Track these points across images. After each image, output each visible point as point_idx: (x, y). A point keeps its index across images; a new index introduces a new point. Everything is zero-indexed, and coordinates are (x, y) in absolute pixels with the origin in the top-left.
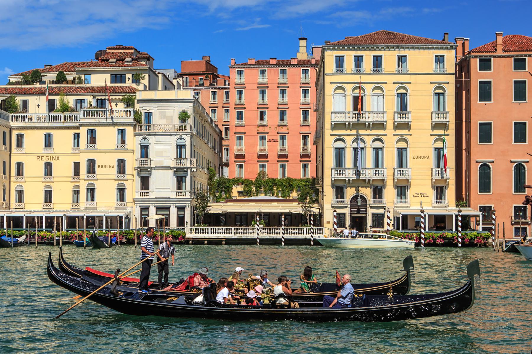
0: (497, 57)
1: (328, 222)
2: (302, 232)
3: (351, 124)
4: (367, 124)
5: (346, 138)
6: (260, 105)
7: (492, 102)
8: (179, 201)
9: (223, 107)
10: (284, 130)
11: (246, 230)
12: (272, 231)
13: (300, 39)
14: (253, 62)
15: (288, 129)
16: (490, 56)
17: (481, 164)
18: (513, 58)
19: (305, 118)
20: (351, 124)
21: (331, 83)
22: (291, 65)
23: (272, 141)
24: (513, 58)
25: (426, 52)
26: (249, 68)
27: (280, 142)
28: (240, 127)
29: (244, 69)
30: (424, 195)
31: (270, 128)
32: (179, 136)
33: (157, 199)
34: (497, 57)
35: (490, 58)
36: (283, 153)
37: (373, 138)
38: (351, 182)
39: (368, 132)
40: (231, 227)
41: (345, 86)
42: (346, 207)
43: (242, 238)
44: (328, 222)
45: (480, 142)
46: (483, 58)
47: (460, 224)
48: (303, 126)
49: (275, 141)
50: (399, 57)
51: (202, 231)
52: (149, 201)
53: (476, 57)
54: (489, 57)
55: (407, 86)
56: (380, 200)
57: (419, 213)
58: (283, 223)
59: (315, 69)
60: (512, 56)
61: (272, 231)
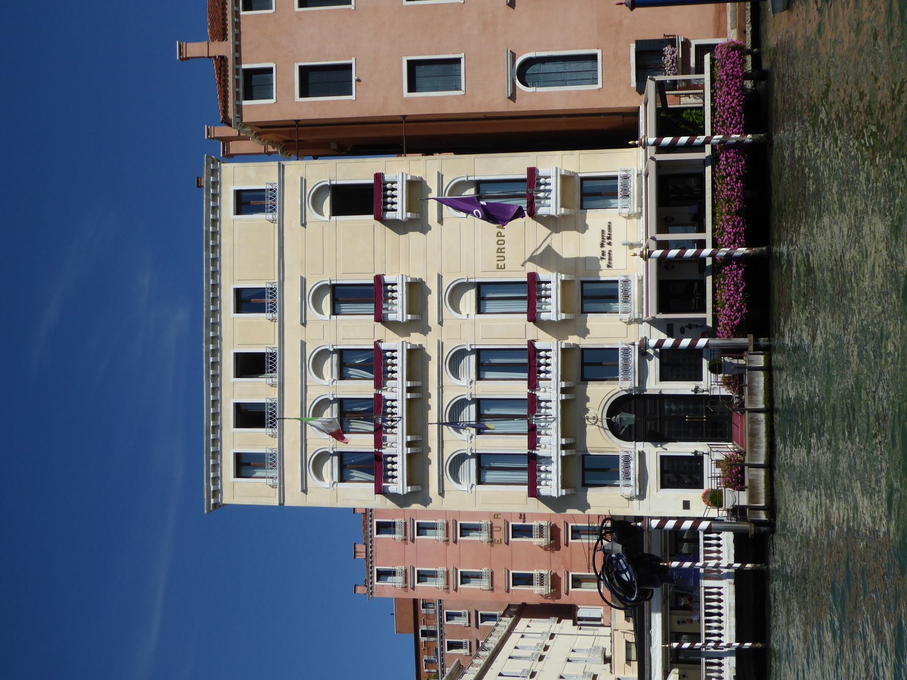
0: (237, 55)
1: (686, 505)
3: (409, 438)
4: (409, 396)
6: (447, 536)
7: (353, 61)
11: (709, 628)
12: (713, 600)
14: (361, 548)
16: (237, 71)
17: (518, 83)
18: (242, 13)
21: (305, 491)
24: (242, 13)
25: (226, 240)
29: (375, 568)
30: (606, 235)
34: (237, 55)
35: (241, 72)
37: (448, 376)
38: (570, 441)
39: (433, 389)
40: (702, 590)
41: (311, 453)
42: (642, 455)
44: (686, 505)
45: (459, 89)
46: (241, 90)
47: (683, 140)
50: (239, 309)
53: (239, 109)
54: (238, 74)
55: (311, 286)
56: (619, 190)
57: (653, 263)
58: (687, 565)
60: (237, 14)
61: (713, 600)
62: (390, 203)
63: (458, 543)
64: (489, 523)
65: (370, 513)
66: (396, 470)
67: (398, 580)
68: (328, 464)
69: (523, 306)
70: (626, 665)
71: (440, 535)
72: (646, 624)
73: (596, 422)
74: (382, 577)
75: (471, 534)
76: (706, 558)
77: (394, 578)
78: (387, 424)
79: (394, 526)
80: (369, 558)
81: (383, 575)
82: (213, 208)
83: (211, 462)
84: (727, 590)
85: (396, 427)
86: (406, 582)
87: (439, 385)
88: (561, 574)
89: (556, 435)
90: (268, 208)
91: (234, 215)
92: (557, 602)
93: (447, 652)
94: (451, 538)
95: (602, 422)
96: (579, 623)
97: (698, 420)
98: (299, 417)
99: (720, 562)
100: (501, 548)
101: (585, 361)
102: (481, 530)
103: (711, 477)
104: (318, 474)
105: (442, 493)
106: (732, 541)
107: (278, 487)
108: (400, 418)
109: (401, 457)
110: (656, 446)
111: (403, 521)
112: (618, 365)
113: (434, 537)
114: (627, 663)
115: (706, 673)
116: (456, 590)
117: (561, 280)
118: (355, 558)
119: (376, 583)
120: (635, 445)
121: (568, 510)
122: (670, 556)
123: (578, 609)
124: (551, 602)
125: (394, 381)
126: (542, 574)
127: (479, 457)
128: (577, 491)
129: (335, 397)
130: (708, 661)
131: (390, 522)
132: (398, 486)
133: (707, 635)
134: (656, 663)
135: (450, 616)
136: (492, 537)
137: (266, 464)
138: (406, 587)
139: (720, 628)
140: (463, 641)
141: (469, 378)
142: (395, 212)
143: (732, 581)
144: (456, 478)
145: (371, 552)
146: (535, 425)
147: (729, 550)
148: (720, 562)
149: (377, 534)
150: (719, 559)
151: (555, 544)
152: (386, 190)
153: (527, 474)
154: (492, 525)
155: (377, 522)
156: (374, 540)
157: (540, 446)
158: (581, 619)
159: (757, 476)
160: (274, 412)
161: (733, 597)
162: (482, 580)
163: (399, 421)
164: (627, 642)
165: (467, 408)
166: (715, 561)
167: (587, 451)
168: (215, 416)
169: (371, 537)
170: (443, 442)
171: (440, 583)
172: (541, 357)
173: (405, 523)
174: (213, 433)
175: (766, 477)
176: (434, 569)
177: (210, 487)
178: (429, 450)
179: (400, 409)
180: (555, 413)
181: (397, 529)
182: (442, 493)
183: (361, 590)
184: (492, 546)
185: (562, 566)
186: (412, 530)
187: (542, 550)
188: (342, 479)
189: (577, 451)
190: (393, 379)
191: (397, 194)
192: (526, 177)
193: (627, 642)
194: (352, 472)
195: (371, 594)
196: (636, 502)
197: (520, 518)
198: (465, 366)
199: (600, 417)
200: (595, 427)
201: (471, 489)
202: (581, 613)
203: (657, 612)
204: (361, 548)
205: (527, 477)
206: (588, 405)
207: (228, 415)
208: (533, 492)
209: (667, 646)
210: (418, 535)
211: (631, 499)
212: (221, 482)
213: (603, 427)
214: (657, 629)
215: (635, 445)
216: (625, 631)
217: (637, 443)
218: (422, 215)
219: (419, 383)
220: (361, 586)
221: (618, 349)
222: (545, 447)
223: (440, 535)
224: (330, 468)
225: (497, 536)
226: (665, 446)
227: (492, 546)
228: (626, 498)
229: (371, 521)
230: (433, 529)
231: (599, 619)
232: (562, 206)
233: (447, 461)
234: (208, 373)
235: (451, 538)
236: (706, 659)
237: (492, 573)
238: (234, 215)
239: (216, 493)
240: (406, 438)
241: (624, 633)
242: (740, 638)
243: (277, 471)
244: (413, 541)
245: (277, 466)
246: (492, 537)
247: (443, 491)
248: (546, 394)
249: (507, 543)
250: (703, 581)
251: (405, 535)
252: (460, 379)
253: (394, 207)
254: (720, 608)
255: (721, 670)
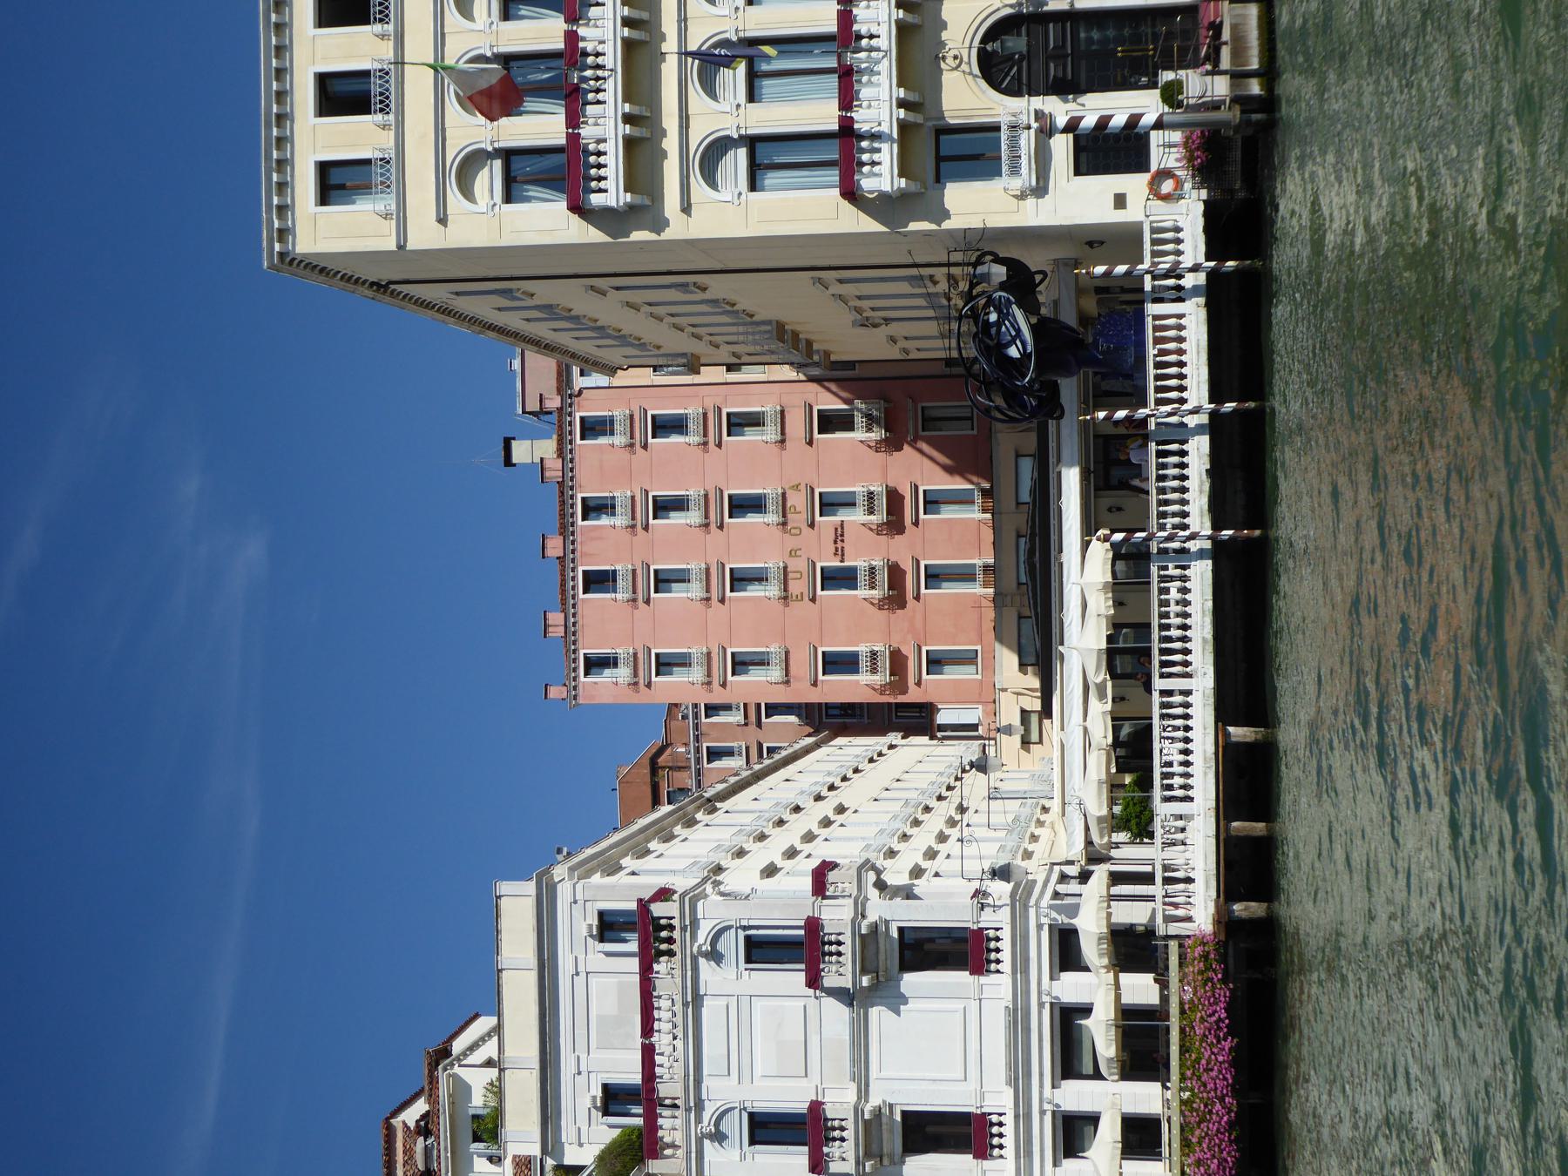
1: (1120, 201)
2: (1172, 321)
3: (627, 107)
5: (700, 133)
6: (708, 591)
8: (1026, 960)
9: (759, 724)
10: (797, 500)
13: (508, 461)
15: (796, 487)
19: (755, 420)
20: (627, 107)
21: (442, 220)
22: (567, 479)
23: (839, 545)
26: (579, 634)
27: (844, 516)
28: (792, 662)
29: (582, 652)
31: (793, 553)
32: (702, 961)
33: (1019, 1075)
36: (882, 503)
38: (913, 97)
39: (670, 122)
43: (1209, 636)
44: (1120, 201)
48: (783, 433)
49: (839, 533)
51: (1172, 358)
52: (1028, 1116)
59: (580, 392)
61: (1174, 664)
62: (592, 154)
63: (727, 602)
64: (781, 565)
65: (572, 556)
66: (605, 166)
67: (623, 673)
68: (484, 173)
69: (833, 176)
70: (1021, 751)
71: (695, 590)
72: (1053, 491)
73: (959, 66)
74: (594, 670)
75: (749, 588)
76: (1154, 254)
77: (615, 671)
78: (589, 85)
79: (615, 580)
80: (570, 634)
81: (596, 664)
82: (279, 162)
83: (275, 177)
84: (1194, 318)
85: (605, 91)
86: (636, 674)
87: (679, 15)
88: (908, 650)
89: (888, 82)
90: (376, 186)
91: (316, 205)
92: (901, 699)
93: (703, 720)
94: (715, 594)
95: (969, 63)
96: (939, 735)
97: (1140, 54)
98: (431, 61)
99: (1180, 258)
100: (802, 609)
101: (942, 154)
102: (767, 580)
103: (1164, 145)
104: (467, 192)
105: (686, 209)
106: (1201, 229)
107: (394, 217)
108: (611, 70)
109: (614, 141)
110: (1066, 101)
111: (630, 567)
112: (1000, 158)
113: (685, 595)
114: (1020, 670)
115: (1157, 469)
116: (724, 685)
117: (898, 119)
118: (545, 636)
119: (582, 679)
120: (1029, 101)
121: (911, 224)
122: (1095, 490)
123: (939, 710)
124: (891, 700)
125: (600, 107)
126: (872, 493)
127: (753, 143)
128: (926, 189)
129: (495, 51)
130: (1160, 447)
131: (607, 571)
132: (612, 193)
133: (1165, 776)
134: (1070, 558)
135: (714, 754)
136: (786, 590)
137: (373, 175)
138: (636, 684)
139: (1184, 639)
140: (735, 744)
141: (736, 186)
142: (601, 8)
143: (1202, 300)
144: (711, 180)
145: (574, 624)
146: (851, 65)
147: (1196, 247)
148: (1180, 258)
149: (584, 593)
150: (1179, 253)
151: (896, 598)
152: (588, 153)
153: (838, 172)
154: (785, 568)
155: (584, 572)
156: (579, 604)
157: (860, 106)
158: (942, 728)
159: (1244, 16)
160: (387, 90)
161: (1204, 329)
162: (770, 667)
163: (609, 76)
164: (1023, 711)
165: (733, 152)
166: (1171, 258)
167: (944, 118)
168: (281, 96)
169: (573, 598)
170: (687, 117)
171: (697, 674)
172: (863, 151)
173: (634, 571)
174: (278, 126)
175: (1260, 18)
176: (685, 650)
177: (273, 222)
178: (664, 133)
179: (612, 57)
180: (887, 43)
181: (620, 583)
182: (686, 209)
183: (556, 692)
184: (787, 605)
185: (909, 637)
186: (645, 583)
187: (874, 610)
188: (508, 198)
189: (926, 119)
190: (600, 191)
191: (608, 187)
192: (836, 30)
193: (1023, 711)
194: (528, 191)
195: (575, 697)
196: (1031, 201)
197: (835, 554)
198: (726, 80)
199: (965, 59)
200: (956, 73)
201: (739, 198)
202: (942, 718)
203: (1071, 465)
204: (556, 618)
205: (838, 178)
206: (945, 35)
207: (304, 94)
208: (851, 193)
209: (1088, 417)
210: (656, 591)
211: (1022, 197)
212: (293, 215)
213: (971, 73)
214: (1072, 498)
215: (1029, 101)
216: (1017, 690)
217: (1032, 98)
218: (653, 201)
219: (645, 15)
220: (556, 685)
221: (996, 128)
222: (869, 106)
223: (695, 590)
224: (489, 179)
225: (796, 587)
226: (1082, 99)
227: (787, 605)
228: (1014, 196)
229: (573, 571)
230: (683, 581)
231: (974, 727)
232: (901, 175)
233: (697, 150)
234: (267, 18)
235: (715, 594)
236: (1158, 444)
237: (787, 653)
238: (315, 116)
239: (283, 234)
240: (623, 107)
241: (1018, 694)
242: (1216, 395)
243: (394, 195)
244: (645, 447)
245: (393, 187)
246: (786, 590)
247: (689, 205)
248: (872, 110)
249: (813, 600)
250: (1150, 305)
251: (634, 592)
252: (718, 191)
253: (602, 184)
254: (1181, 352)
255: (1184, 487)
